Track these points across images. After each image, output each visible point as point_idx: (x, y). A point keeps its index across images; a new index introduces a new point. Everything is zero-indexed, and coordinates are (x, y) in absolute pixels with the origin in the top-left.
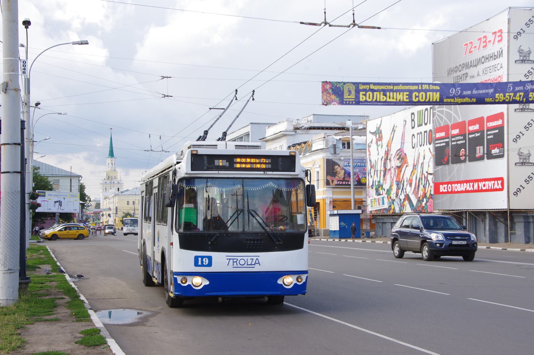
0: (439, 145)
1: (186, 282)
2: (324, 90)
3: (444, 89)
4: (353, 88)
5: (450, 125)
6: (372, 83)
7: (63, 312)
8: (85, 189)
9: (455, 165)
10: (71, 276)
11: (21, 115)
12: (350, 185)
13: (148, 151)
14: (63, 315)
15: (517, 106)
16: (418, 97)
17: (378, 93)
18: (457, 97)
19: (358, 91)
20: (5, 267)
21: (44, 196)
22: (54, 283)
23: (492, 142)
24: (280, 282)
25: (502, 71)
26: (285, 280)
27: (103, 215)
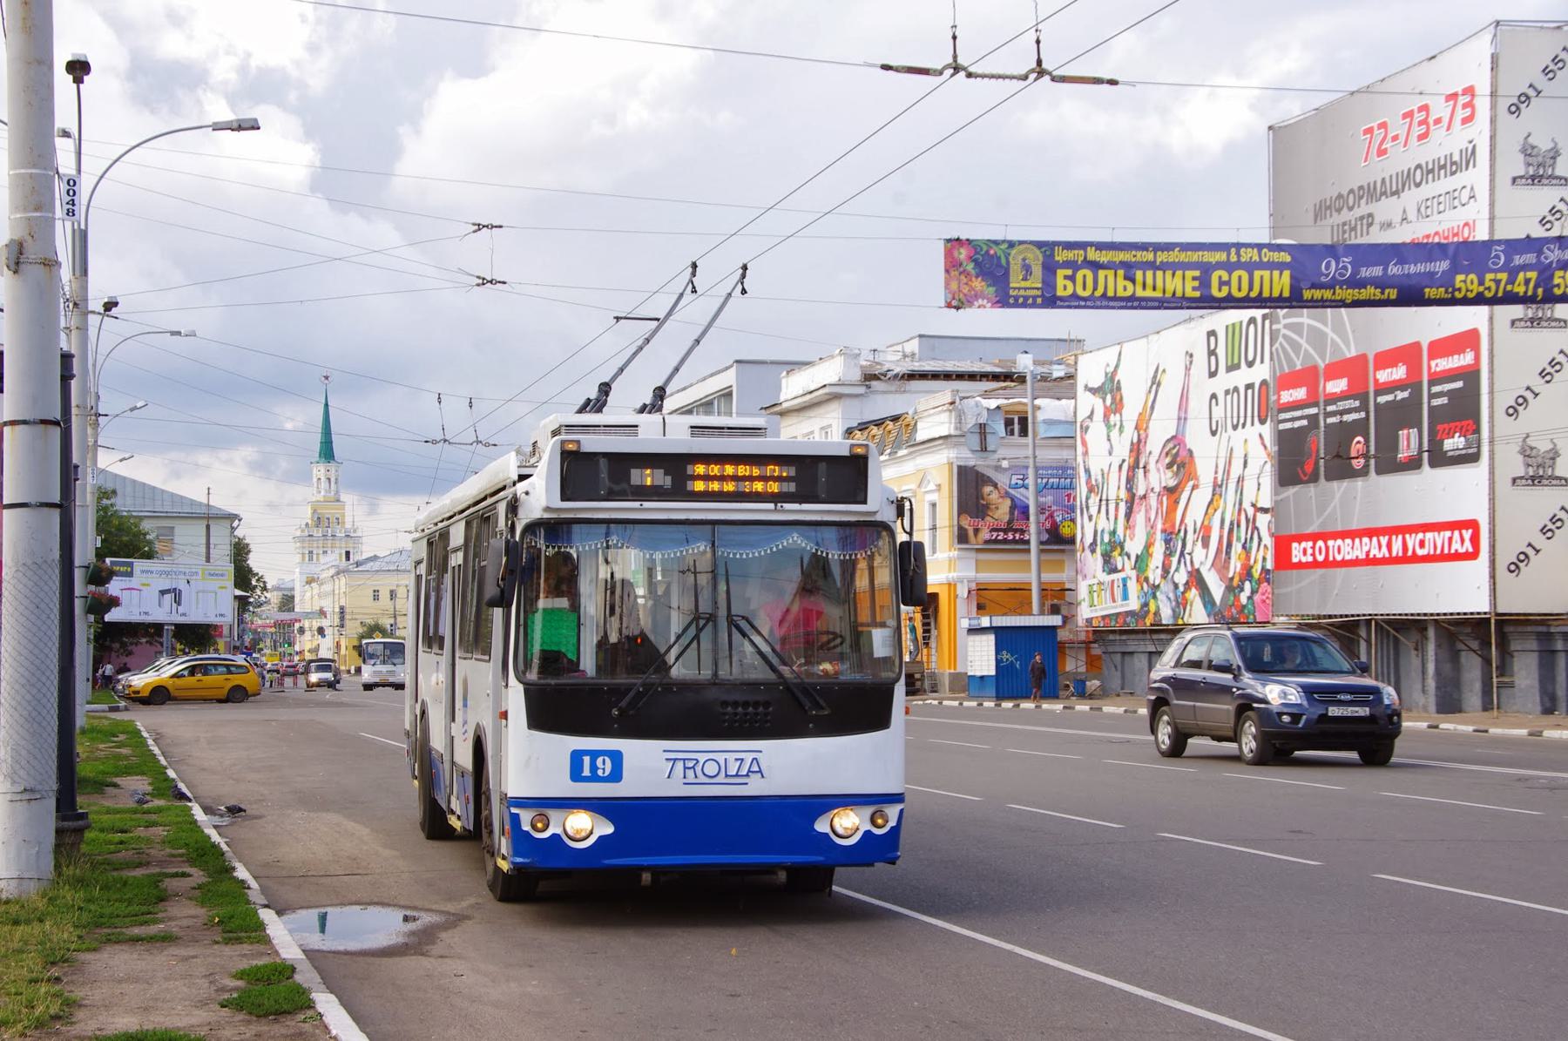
0: (1288, 425)
1: (547, 826)
2: (952, 265)
3: (1304, 260)
4: (1036, 259)
5: (1322, 365)
6: (1091, 244)
7: (184, 914)
8: (251, 556)
9: (1335, 484)
10: (208, 810)
11: (63, 336)
12: (1028, 542)
13: (435, 442)
14: (185, 923)
15: (1517, 311)
16: (1228, 283)
17: (1110, 273)
18: (1341, 284)
19: (1050, 268)
20: (14, 782)
21: (130, 574)
22: (160, 832)
23: (1446, 417)
24: (821, 826)
25: (1474, 207)
26: (836, 820)
27: (302, 631)
